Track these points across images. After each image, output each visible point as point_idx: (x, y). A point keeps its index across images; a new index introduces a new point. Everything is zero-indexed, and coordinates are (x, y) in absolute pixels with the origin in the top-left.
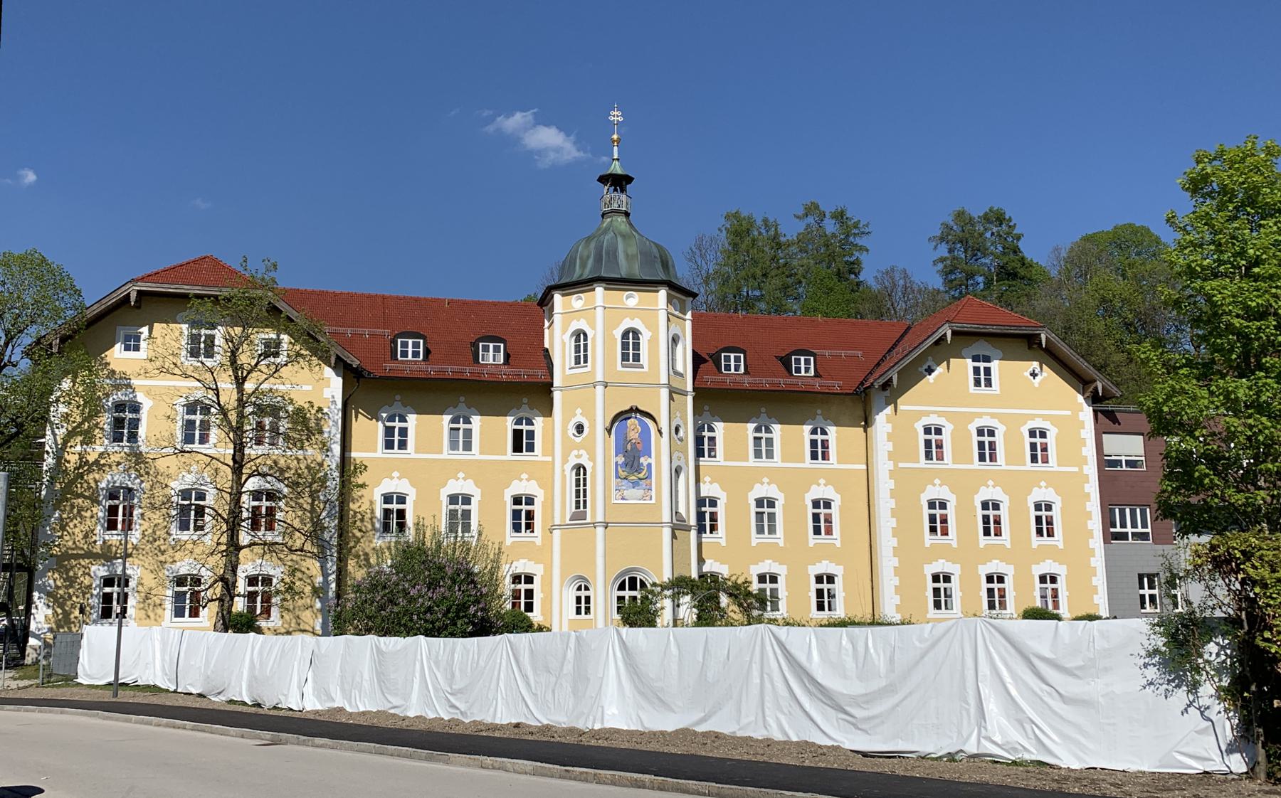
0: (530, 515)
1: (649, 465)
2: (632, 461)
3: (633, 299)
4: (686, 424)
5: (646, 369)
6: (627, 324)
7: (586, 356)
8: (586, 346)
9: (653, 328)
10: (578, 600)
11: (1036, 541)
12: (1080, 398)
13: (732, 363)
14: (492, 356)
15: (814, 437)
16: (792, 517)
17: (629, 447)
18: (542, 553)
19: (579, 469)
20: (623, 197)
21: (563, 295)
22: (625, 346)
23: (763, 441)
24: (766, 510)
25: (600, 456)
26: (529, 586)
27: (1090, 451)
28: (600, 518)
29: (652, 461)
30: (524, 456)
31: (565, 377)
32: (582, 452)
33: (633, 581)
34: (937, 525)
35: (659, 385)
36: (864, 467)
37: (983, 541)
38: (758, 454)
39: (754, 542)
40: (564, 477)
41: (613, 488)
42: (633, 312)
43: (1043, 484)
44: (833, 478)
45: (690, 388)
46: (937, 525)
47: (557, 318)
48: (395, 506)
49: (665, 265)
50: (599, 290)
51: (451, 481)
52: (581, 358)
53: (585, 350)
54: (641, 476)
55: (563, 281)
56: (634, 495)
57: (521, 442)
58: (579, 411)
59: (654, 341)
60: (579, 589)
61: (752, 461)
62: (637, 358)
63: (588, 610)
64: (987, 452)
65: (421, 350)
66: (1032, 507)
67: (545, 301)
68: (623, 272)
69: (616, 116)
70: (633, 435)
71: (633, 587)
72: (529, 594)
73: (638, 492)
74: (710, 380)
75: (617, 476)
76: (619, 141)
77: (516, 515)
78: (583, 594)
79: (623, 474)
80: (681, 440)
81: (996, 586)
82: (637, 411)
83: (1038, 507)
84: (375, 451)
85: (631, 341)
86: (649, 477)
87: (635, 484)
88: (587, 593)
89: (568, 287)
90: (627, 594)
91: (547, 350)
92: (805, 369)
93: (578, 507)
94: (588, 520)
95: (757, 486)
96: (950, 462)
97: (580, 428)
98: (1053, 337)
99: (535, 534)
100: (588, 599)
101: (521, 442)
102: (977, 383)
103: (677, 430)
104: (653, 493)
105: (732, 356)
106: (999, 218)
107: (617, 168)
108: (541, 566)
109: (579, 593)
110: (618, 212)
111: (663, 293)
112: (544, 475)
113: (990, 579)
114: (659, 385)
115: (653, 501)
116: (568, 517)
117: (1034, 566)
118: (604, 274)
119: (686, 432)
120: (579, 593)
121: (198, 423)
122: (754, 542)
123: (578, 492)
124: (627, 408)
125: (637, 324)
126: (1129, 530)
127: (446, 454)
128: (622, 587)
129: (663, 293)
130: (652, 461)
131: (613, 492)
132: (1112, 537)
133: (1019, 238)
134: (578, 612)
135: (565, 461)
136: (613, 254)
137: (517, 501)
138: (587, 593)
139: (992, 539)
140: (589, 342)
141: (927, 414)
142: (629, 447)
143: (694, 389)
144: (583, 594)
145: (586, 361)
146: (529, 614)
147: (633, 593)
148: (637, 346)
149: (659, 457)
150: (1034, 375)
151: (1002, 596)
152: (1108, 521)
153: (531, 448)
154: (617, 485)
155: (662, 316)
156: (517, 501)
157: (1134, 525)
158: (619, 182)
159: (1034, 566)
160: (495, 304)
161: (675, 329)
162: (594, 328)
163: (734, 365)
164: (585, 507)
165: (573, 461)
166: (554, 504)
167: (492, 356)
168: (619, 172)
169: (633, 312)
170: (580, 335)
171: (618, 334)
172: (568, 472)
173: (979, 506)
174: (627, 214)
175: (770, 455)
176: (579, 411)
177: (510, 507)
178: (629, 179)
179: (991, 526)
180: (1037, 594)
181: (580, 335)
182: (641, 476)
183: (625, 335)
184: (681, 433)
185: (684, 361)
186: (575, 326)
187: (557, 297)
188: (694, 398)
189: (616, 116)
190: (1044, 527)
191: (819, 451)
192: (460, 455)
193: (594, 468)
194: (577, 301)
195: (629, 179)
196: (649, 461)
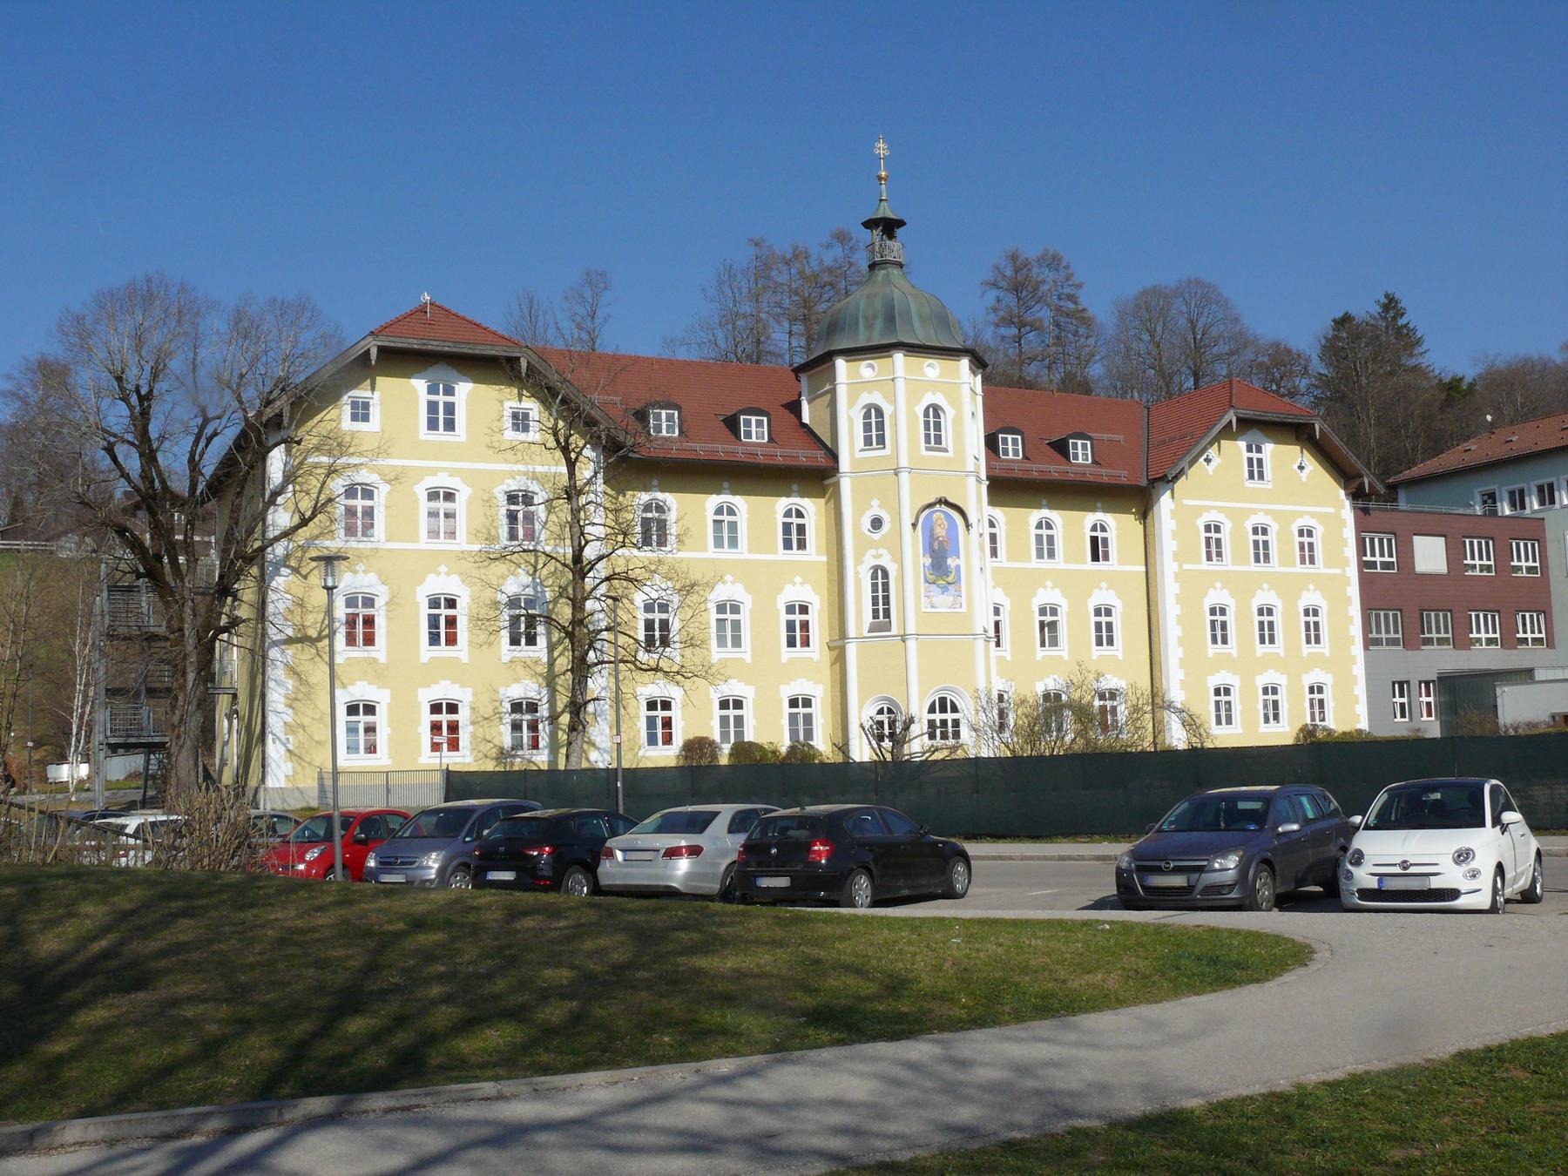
1: (958, 567)
3: (932, 368)
5: (951, 454)
6: (930, 399)
9: (956, 403)
11: (426, 652)
12: (1342, 493)
13: (1010, 447)
14: (756, 431)
17: (936, 545)
23: (725, 526)
24: (729, 616)
26: (666, 714)
27: (1351, 551)
29: (962, 562)
30: (1101, 565)
31: (854, 461)
32: (881, 551)
33: (943, 701)
34: (1220, 633)
36: (1143, 569)
37: (787, 654)
38: (718, 542)
40: (858, 582)
42: (933, 385)
44: (1114, 581)
46: (1220, 633)
50: (899, 357)
51: (431, 578)
54: (950, 579)
56: (943, 601)
58: (875, 502)
59: (958, 420)
62: (938, 439)
64: (1262, 552)
69: (881, 148)
70: (941, 532)
71: (943, 710)
72: (808, 719)
73: (948, 599)
77: (434, 622)
81: (732, 713)
82: (947, 503)
83: (1213, 611)
86: (958, 580)
87: (944, 590)
90: (938, 717)
92: (1082, 453)
94: (894, 631)
96: (464, 541)
98: (1328, 430)
102: (433, 425)
104: (964, 600)
105: (753, 419)
106: (1054, 262)
107: (886, 211)
111: (965, 362)
113: (793, 703)
115: (964, 610)
116: (866, 627)
117: (420, 691)
121: (360, 510)
126: (1384, 636)
127: (424, 542)
128: (932, 710)
129: (965, 362)
130: (962, 562)
132: (1369, 643)
133: (1079, 286)
139: (443, 650)
141: (433, 472)
142: (936, 545)
143: (988, 478)
147: (944, 716)
150: (1301, 468)
151: (1229, 710)
152: (1367, 628)
153: (1106, 558)
154: (927, 591)
157: (1388, 632)
158: (889, 227)
159: (420, 691)
162: (894, 402)
165: (870, 561)
169: (933, 385)
173: (783, 610)
175: (733, 542)
176: (875, 502)
178: (901, 223)
179: (1267, 634)
182: (950, 579)
186: (866, 399)
187: (840, 363)
189: (881, 148)
190: (1313, 634)
191: (1046, 548)
194: (867, 369)
195: (901, 223)
196: (957, 562)
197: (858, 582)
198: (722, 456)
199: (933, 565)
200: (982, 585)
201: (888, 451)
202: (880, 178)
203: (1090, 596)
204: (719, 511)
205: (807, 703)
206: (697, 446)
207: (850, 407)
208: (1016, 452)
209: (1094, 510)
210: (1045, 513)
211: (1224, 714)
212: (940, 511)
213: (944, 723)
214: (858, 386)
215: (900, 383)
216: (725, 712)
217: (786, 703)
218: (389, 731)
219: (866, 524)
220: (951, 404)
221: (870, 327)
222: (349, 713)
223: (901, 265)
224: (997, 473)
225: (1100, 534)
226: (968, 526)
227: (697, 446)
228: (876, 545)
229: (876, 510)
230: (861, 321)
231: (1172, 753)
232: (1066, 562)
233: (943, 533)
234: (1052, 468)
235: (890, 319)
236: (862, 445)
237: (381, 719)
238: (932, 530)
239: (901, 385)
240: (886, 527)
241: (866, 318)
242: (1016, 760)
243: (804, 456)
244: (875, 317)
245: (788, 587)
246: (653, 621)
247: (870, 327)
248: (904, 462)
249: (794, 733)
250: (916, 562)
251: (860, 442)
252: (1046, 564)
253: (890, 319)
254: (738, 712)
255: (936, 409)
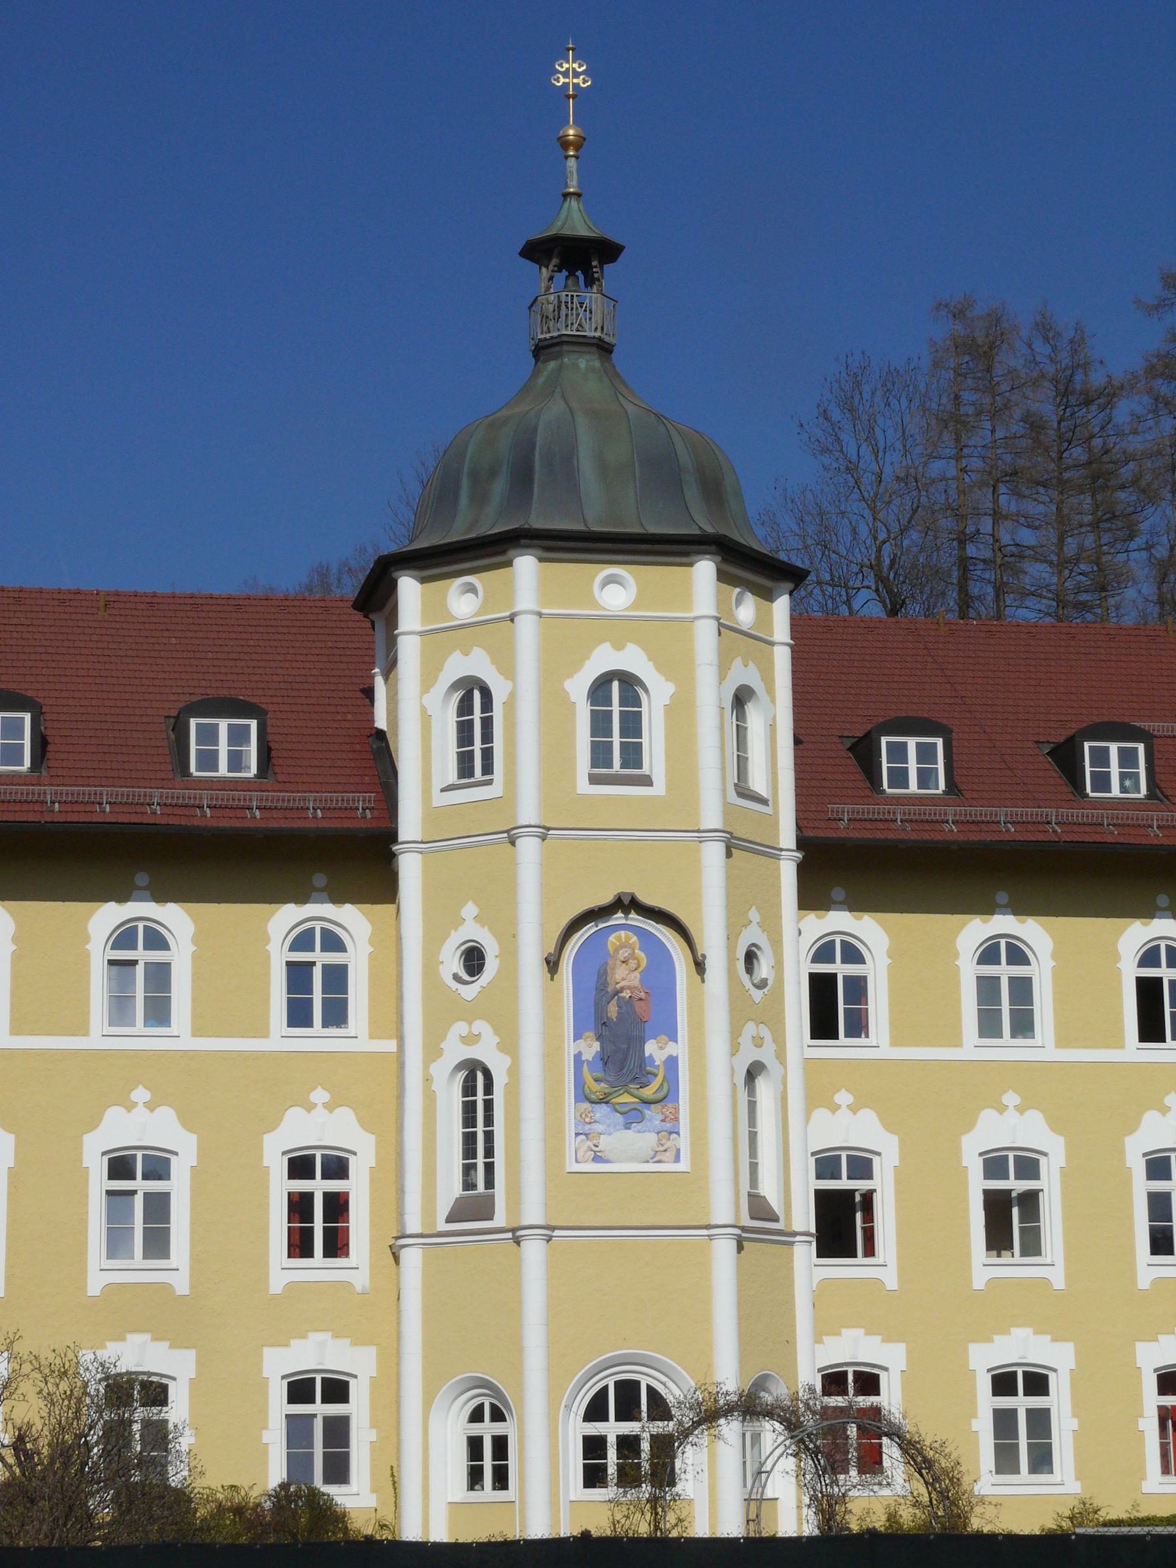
0: (337, 1206)
1: (672, 1062)
2: (622, 1053)
3: (617, 588)
4: (777, 944)
5: (659, 788)
7: (488, 755)
8: (487, 724)
9: (678, 667)
10: (475, 1445)
11: (282, 1271)
15: (989, 970)
16: (230, 1204)
17: (613, 1010)
18: (375, 1319)
19: (475, 1075)
20: (592, 297)
21: (423, 580)
22: (600, 723)
25: (538, 1041)
28: (533, 1214)
29: (680, 1049)
31: (431, 815)
33: (628, 1391)
35: (702, 834)
38: (989, 1026)
39: (96, 1283)
40: (430, 1098)
41: (570, 1127)
42: (618, 628)
43: (320, 1096)
45: (787, 837)
47: (409, 650)
48: (1015, 1185)
49: (714, 490)
50: (526, 565)
52: (475, 756)
53: (487, 737)
54: (648, 1092)
55: (423, 543)
56: (628, 1147)
57: (315, 994)
58: (470, 910)
59: (681, 711)
60: (476, 1416)
61: (279, 1035)
62: (633, 755)
63: (501, 1479)
65: (27, 742)
66: (1139, 1169)
67: (376, 597)
68: (594, 517)
69: (571, 73)
70: (625, 978)
71: (627, 1411)
72: (338, 1431)
73: (642, 1139)
74: (847, 818)
75: (582, 1095)
76: (579, 144)
78: (487, 1430)
79: (598, 1089)
80: (761, 985)
81: (1021, 1403)
84: (957, 1042)
85: (616, 709)
86: (668, 1096)
87: (632, 1118)
88: (499, 1428)
89: (439, 560)
90: (612, 1429)
91: (381, 735)
92: (1118, 775)
93: (469, 1185)
95: (987, 1116)
97: (474, 959)
99: (173, 1262)
100: (501, 1444)
101: (315, 994)
103: (750, 958)
104: (684, 1141)
105: (912, 743)
107: (575, 221)
108: (191, 1355)
109: (476, 1429)
110: (581, 343)
111: (705, 569)
112: (378, 1091)
113: (1003, 1383)
114: (702, 834)
115: (683, 1166)
116: (444, 1208)
117: (1140, 1347)
118: (538, 522)
119: (778, 966)
120: (476, 1429)
122: (96, 1283)
123: (469, 1141)
124: (606, 898)
125: (632, 660)
127: (99, 1034)
128: (596, 1411)
129: (705, 569)
130: (680, 1049)
131: (571, 1143)
134: (475, 1477)
135: (432, 1052)
136: (564, 467)
137: (300, 1167)
138: (499, 1428)
140: (498, 713)
142: (613, 1010)
144: (487, 1430)
145: (488, 768)
146: (331, 1490)
147: (629, 1428)
148: (632, 725)
149: (702, 1037)
153: (858, 1026)
154: (581, 1119)
155: (705, 638)
156: (300, 1167)
158: (581, 257)
159: (1140, 1347)
160: (113, 600)
161: (744, 674)
163: (915, 769)
164: (490, 1183)
165: (455, 1052)
166: (406, 1172)
167: (225, 751)
168: (583, 231)
169: (618, 628)
170: (472, 695)
171: (578, 687)
172: (439, 1085)
174: (604, 348)
175: (1023, 1025)
176: (470, 910)
177: (280, 1187)
178: (608, 251)
180: (275, 1438)
181: (472, 695)
182: (648, 1092)
183: (599, 689)
184: (764, 969)
185: (773, 765)
186: (458, 666)
187: (408, 588)
188: (803, 870)
189: (571, 73)
191: (1007, 1007)
192: (140, 1038)
193: (514, 1072)
194: (462, 598)
195: (608, 251)
196: (671, 1049)
197: (430, 1098)
198: (106, 812)
199: (605, 1059)
200: (757, 1112)
201: (496, 789)
202: (565, 144)
203: (969, 1125)
204: (989, 955)
205: (1037, 1384)
206: (1001, 814)
207: (427, 683)
208: (925, 778)
209: (988, 909)
210: (1004, 924)
211: (1024, 1440)
212: (623, 933)
213: (628, 1444)
214: (445, 635)
215: (527, 628)
216: (1005, 1402)
217: (985, 1384)
218: (1074, 1424)
219: (453, 964)
220: (662, 667)
221: (480, 498)
222: (292, 1399)
223: (604, 348)
224: (810, 833)
225: (841, 969)
226: (700, 966)
227: (1001, 814)
228: (469, 1012)
229: (472, 931)
230: (465, 484)
231: (775, 1543)
232: (1061, 1043)
233: (635, 979)
234: (1052, 813)
235: (522, 477)
236: (452, 776)
237: (1059, 1400)
238: (603, 976)
239: (527, 631)
240: (491, 966)
241: (475, 476)
242: (40, 1549)
243: (315, 807)
244: (493, 473)
245: (294, 1115)
246: (308, 1198)
247: (480, 498)
248: (528, 812)
249: (298, 1463)
250: (551, 1056)
251: (449, 771)
252: (1007, 1049)
253: (522, 477)
254: (1037, 1402)
255: (629, 683)
